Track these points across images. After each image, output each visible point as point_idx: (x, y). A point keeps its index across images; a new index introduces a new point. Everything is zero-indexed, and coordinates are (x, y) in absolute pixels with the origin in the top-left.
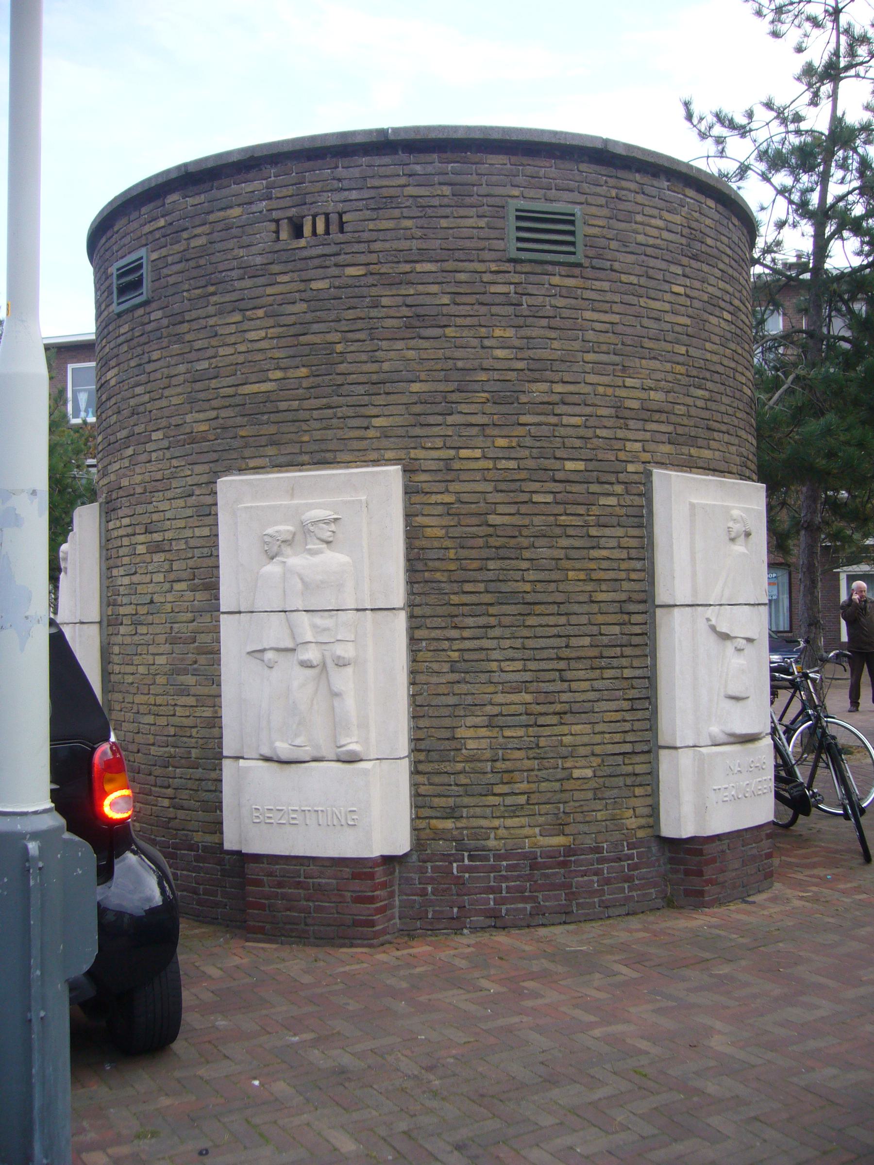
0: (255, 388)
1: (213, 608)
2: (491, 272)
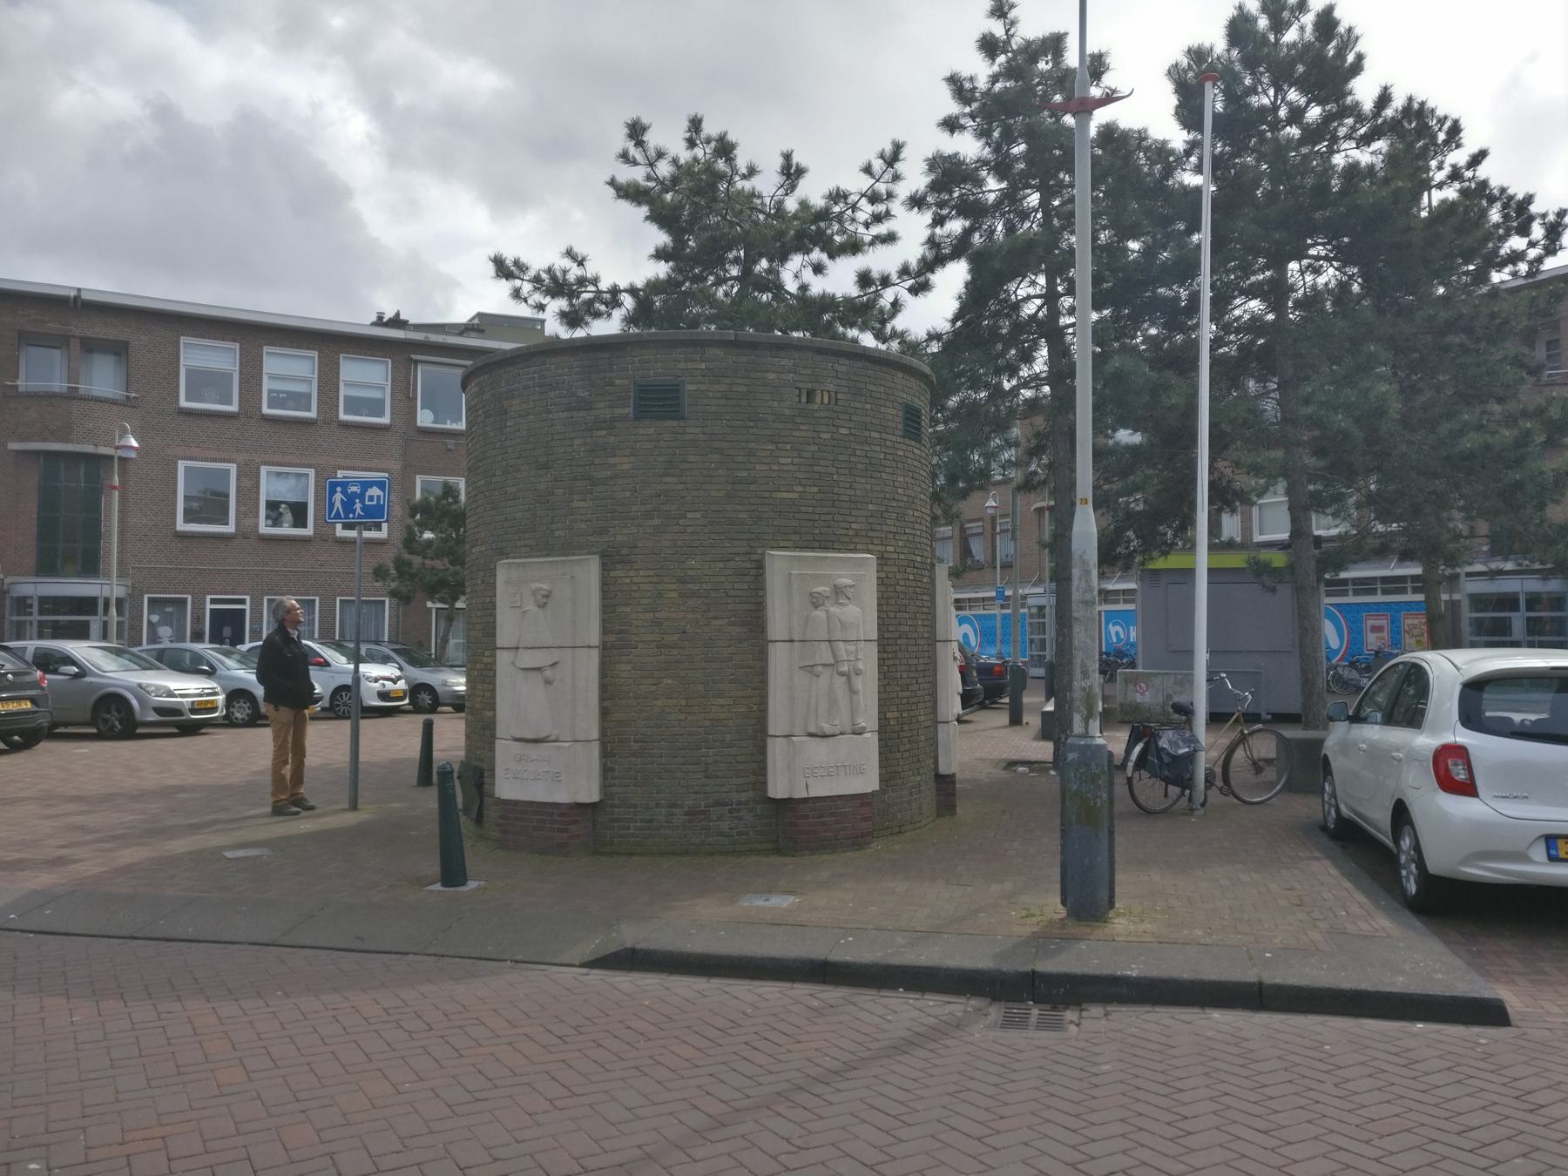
0: (784, 495)
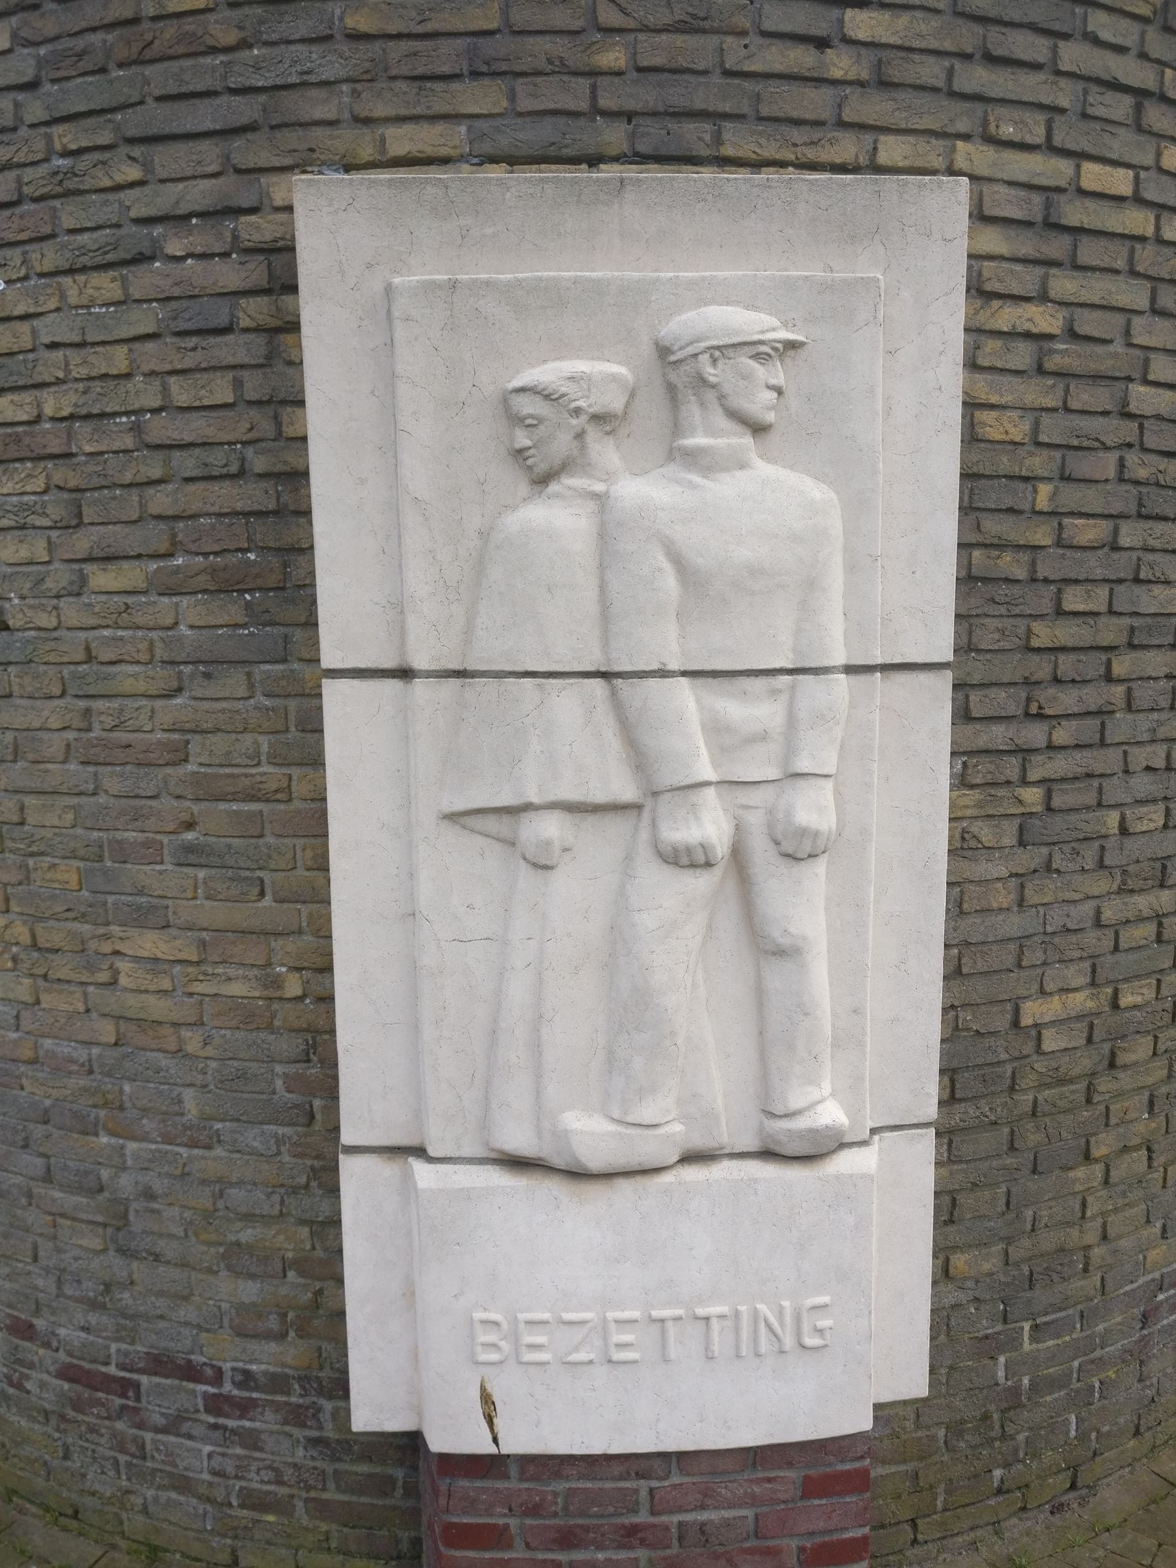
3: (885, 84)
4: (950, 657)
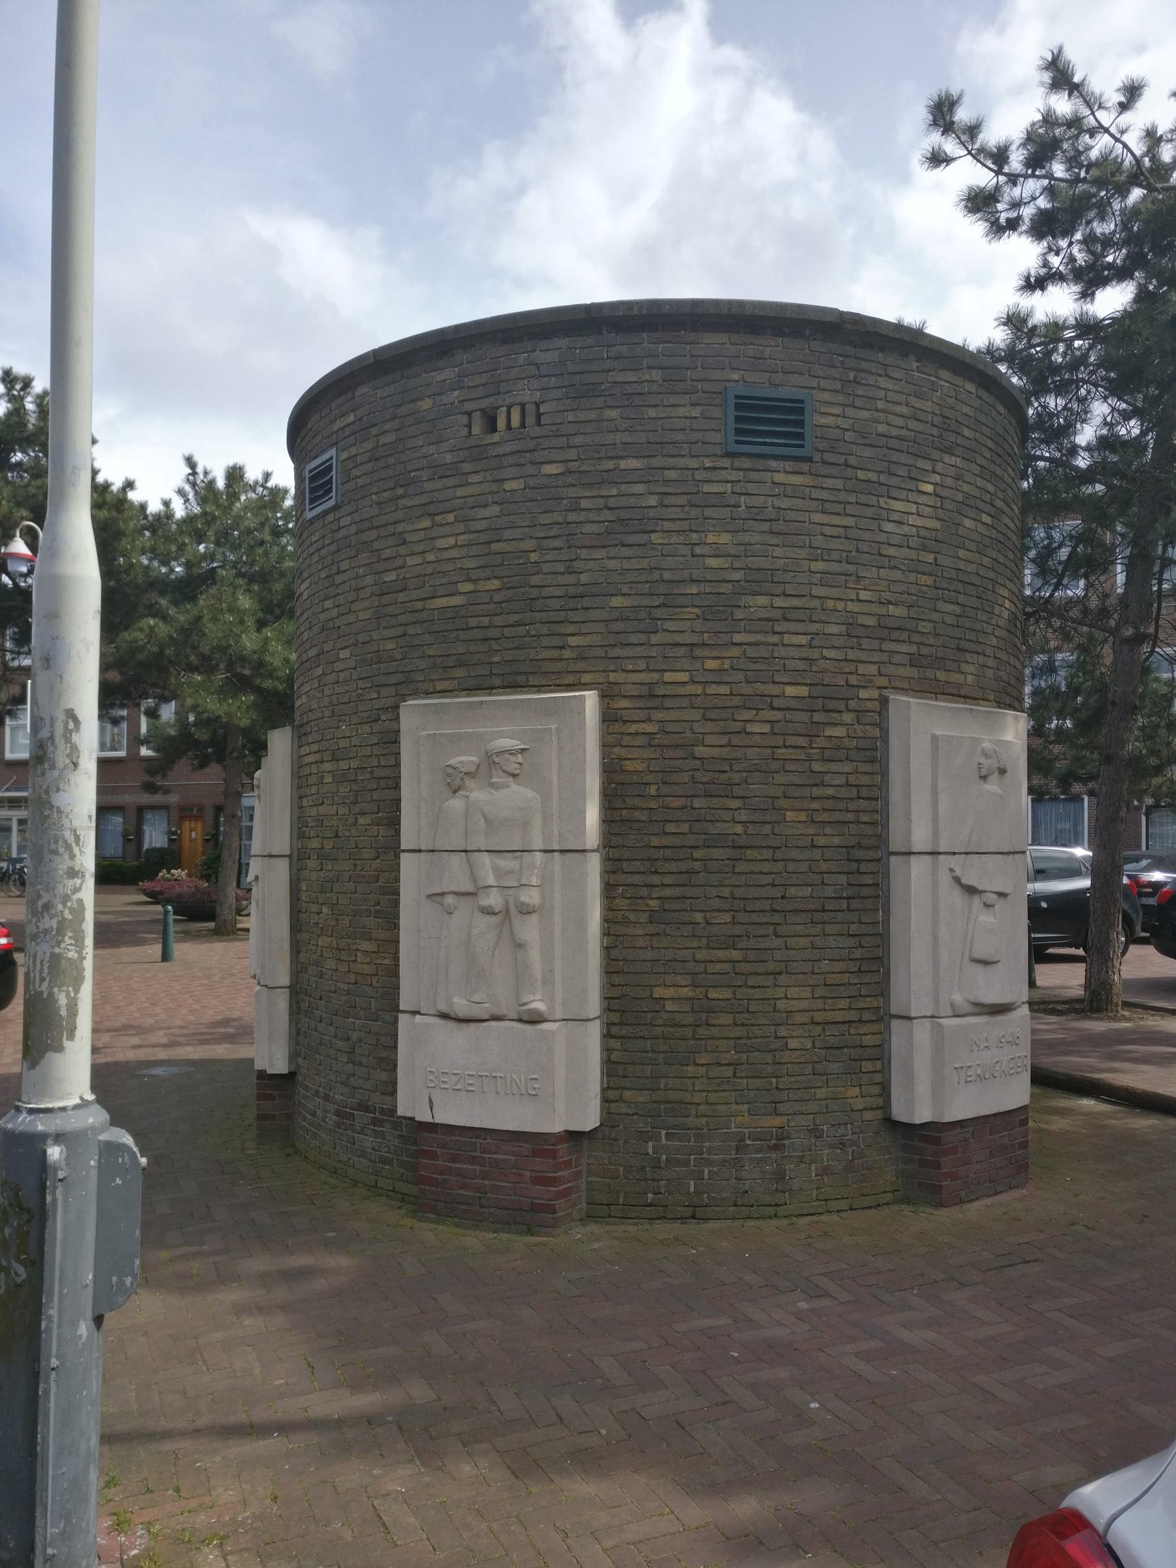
1: (393, 848)
2: (705, 469)
3: (584, 658)
4: (893, 859)
